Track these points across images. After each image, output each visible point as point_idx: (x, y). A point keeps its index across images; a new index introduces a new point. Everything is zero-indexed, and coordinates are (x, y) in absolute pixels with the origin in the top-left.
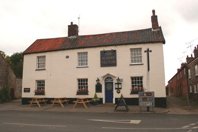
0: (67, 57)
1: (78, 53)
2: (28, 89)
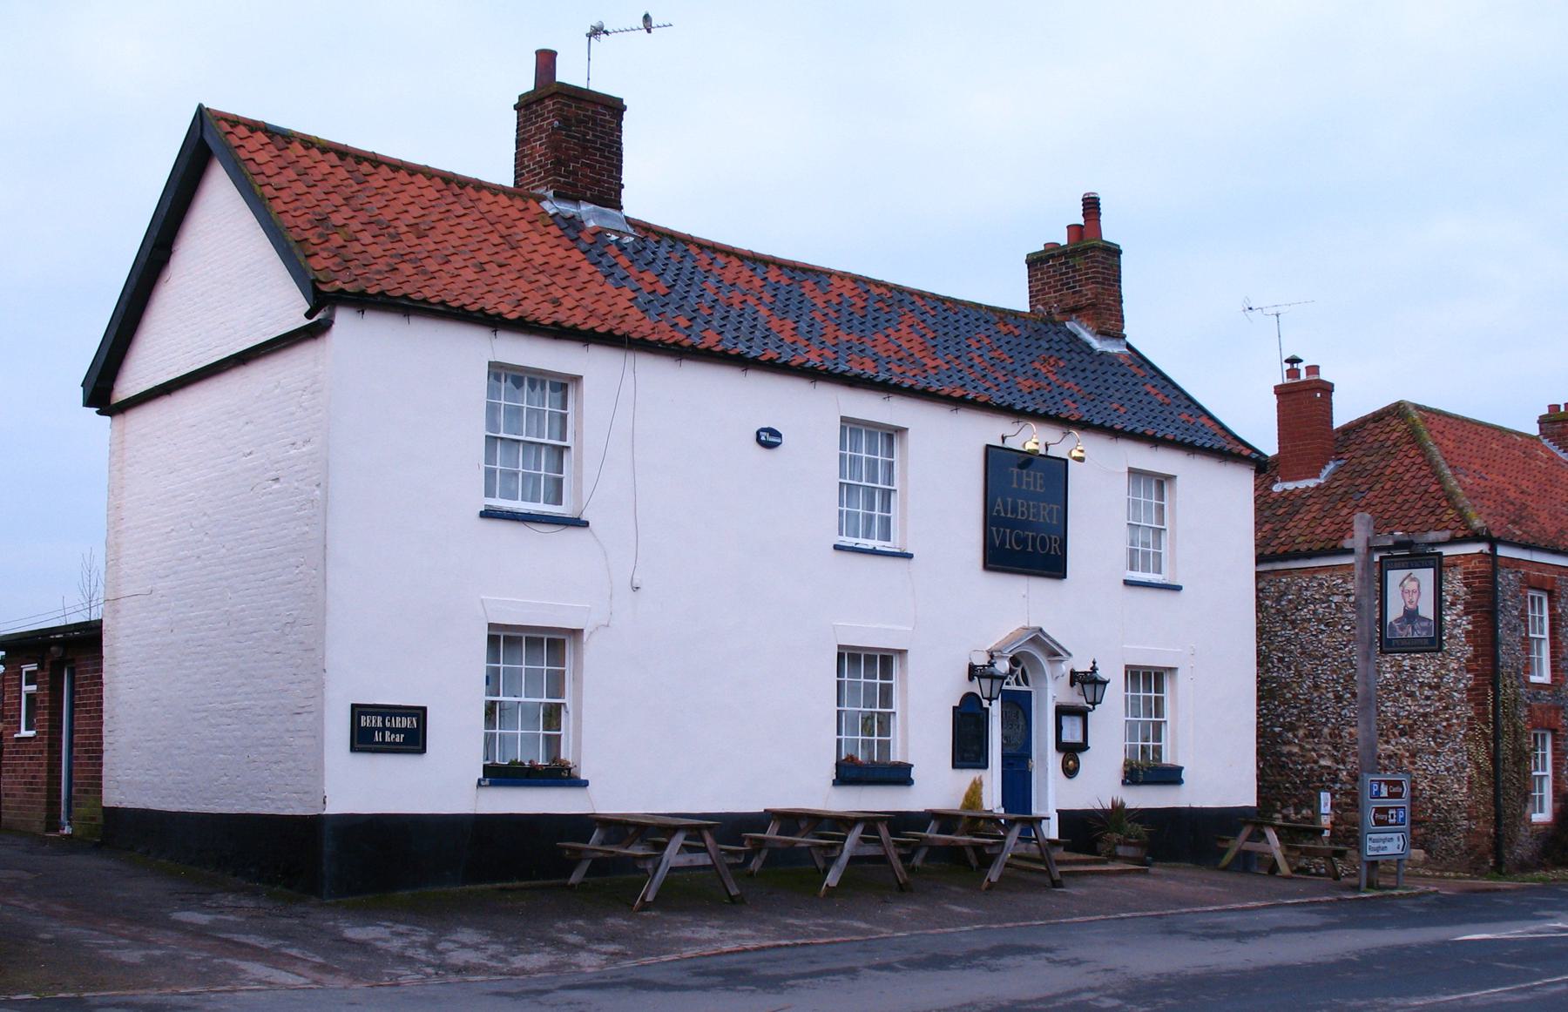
0: (768, 439)
1: (497, 370)
2: (405, 722)
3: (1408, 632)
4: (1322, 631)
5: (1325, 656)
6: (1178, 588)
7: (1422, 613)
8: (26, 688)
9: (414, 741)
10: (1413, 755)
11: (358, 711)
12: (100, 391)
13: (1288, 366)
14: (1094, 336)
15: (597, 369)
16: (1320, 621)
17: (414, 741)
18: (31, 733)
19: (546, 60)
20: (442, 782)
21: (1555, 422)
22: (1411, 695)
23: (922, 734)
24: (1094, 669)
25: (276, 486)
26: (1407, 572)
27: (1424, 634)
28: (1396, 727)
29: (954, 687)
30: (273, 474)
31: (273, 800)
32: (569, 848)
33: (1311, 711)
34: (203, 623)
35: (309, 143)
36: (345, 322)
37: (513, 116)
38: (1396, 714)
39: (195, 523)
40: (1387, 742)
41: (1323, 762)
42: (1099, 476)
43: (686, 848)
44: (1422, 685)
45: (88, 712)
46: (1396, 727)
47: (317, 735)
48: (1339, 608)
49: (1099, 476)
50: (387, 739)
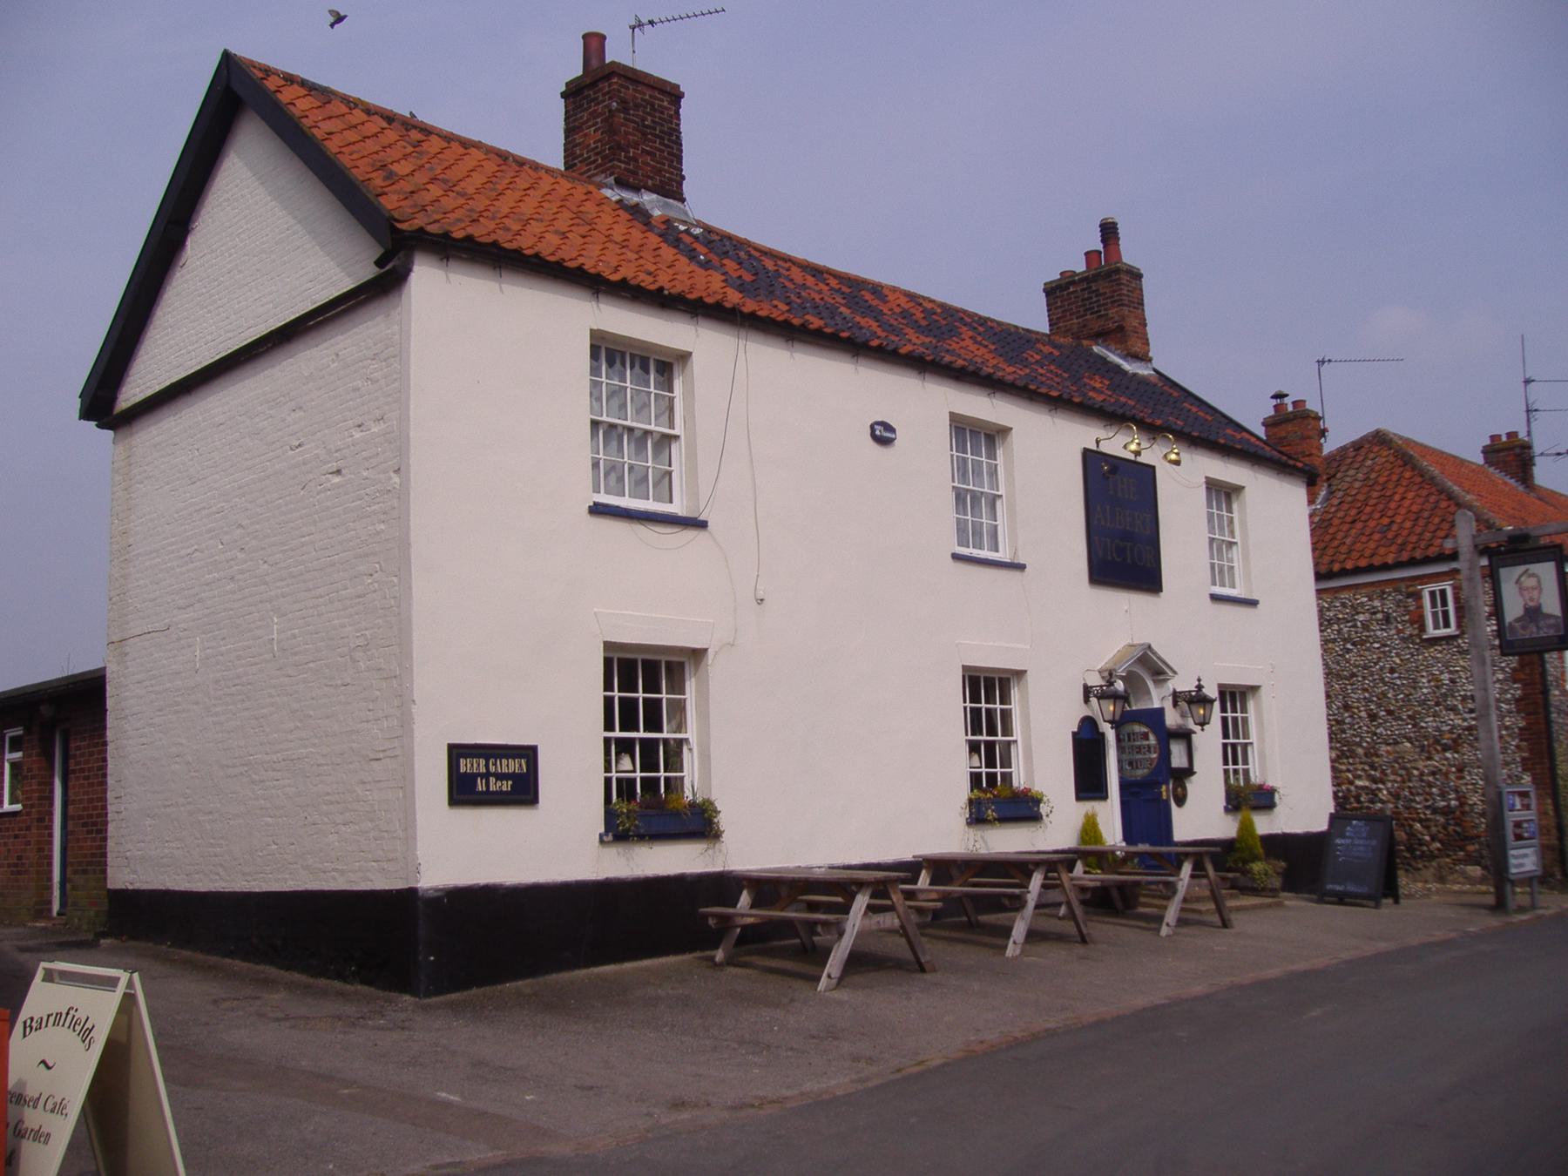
3: (1532, 632)
4: (1348, 651)
5: (1353, 675)
6: (1253, 603)
7: (1546, 609)
8: (12, 756)
9: (524, 791)
10: (1460, 770)
11: (457, 752)
12: (101, 402)
13: (1274, 402)
14: (1124, 358)
15: (704, 344)
16: (1345, 640)
17: (524, 791)
18: (18, 807)
19: (594, 43)
20: (558, 842)
21: (1499, 451)
22: (1453, 709)
23: (1043, 763)
24: (1200, 687)
25: (336, 479)
26: (1521, 569)
27: (1552, 632)
28: (1437, 742)
29: (1072, 712)
30: (334, 466)
31: (342, 872)
32: (714, 915)
33: (1344, 731)
34: (239, 658)
35: (352, 103)
36: (426, 277)
37: (559, 106)
38: (1438, 729)
39: (226, 538)
40: (1429, 758)
41: (1359, 783)
42: (1181, 480)
43: (871, 909)
44: (1464, 698)
45: (87, 778)
46: (1437, 742)
47: (405, 783)
48: (1366, 626)
49: (1181, 480)
50: (492, 788)
